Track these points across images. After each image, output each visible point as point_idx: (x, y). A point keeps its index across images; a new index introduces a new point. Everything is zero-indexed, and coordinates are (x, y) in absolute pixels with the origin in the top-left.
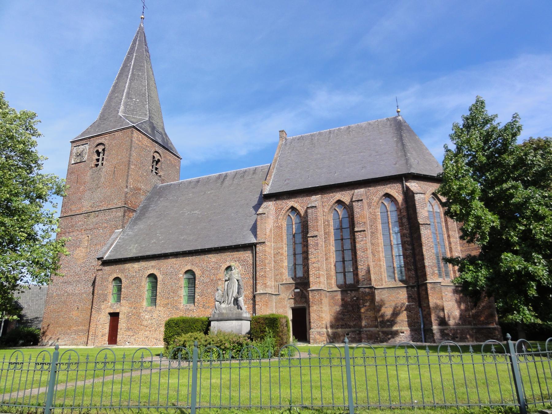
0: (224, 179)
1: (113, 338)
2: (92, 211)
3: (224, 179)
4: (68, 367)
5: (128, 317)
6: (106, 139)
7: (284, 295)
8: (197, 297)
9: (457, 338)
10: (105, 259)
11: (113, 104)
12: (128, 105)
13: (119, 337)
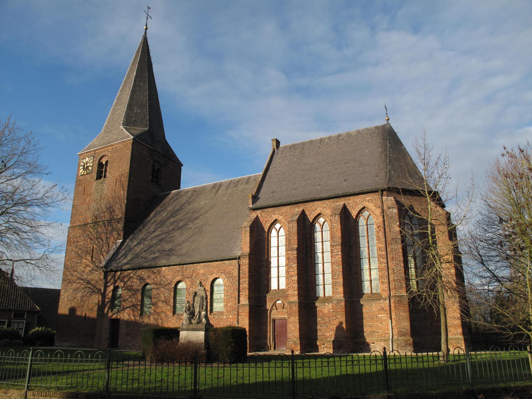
0: (218, 189)
3: (218, 189)
4: (340, 358)
9: (426, 348)
11: (116, 117)
12: (129, 117)
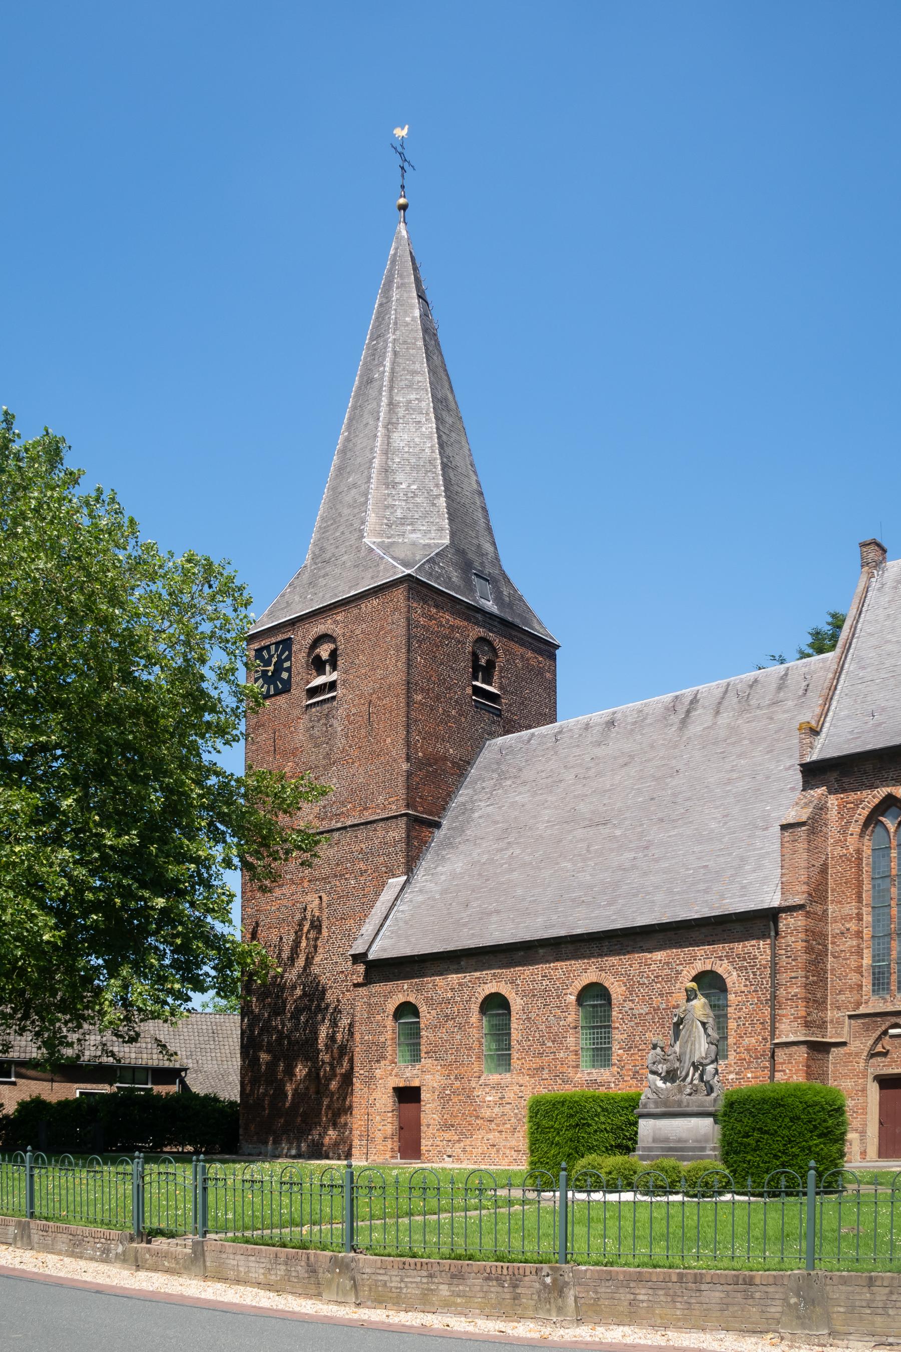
0: (688, 712)
1: (409, 1143)
2: (321, 829)
5: (444, 1099)
6: (336, 622)
7: (858, 1043)
8: (617, 1051)
10: (371, 957)
11: (346, 511)
13: (425, 1144)
